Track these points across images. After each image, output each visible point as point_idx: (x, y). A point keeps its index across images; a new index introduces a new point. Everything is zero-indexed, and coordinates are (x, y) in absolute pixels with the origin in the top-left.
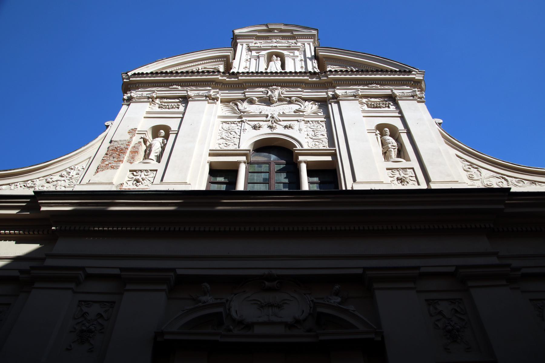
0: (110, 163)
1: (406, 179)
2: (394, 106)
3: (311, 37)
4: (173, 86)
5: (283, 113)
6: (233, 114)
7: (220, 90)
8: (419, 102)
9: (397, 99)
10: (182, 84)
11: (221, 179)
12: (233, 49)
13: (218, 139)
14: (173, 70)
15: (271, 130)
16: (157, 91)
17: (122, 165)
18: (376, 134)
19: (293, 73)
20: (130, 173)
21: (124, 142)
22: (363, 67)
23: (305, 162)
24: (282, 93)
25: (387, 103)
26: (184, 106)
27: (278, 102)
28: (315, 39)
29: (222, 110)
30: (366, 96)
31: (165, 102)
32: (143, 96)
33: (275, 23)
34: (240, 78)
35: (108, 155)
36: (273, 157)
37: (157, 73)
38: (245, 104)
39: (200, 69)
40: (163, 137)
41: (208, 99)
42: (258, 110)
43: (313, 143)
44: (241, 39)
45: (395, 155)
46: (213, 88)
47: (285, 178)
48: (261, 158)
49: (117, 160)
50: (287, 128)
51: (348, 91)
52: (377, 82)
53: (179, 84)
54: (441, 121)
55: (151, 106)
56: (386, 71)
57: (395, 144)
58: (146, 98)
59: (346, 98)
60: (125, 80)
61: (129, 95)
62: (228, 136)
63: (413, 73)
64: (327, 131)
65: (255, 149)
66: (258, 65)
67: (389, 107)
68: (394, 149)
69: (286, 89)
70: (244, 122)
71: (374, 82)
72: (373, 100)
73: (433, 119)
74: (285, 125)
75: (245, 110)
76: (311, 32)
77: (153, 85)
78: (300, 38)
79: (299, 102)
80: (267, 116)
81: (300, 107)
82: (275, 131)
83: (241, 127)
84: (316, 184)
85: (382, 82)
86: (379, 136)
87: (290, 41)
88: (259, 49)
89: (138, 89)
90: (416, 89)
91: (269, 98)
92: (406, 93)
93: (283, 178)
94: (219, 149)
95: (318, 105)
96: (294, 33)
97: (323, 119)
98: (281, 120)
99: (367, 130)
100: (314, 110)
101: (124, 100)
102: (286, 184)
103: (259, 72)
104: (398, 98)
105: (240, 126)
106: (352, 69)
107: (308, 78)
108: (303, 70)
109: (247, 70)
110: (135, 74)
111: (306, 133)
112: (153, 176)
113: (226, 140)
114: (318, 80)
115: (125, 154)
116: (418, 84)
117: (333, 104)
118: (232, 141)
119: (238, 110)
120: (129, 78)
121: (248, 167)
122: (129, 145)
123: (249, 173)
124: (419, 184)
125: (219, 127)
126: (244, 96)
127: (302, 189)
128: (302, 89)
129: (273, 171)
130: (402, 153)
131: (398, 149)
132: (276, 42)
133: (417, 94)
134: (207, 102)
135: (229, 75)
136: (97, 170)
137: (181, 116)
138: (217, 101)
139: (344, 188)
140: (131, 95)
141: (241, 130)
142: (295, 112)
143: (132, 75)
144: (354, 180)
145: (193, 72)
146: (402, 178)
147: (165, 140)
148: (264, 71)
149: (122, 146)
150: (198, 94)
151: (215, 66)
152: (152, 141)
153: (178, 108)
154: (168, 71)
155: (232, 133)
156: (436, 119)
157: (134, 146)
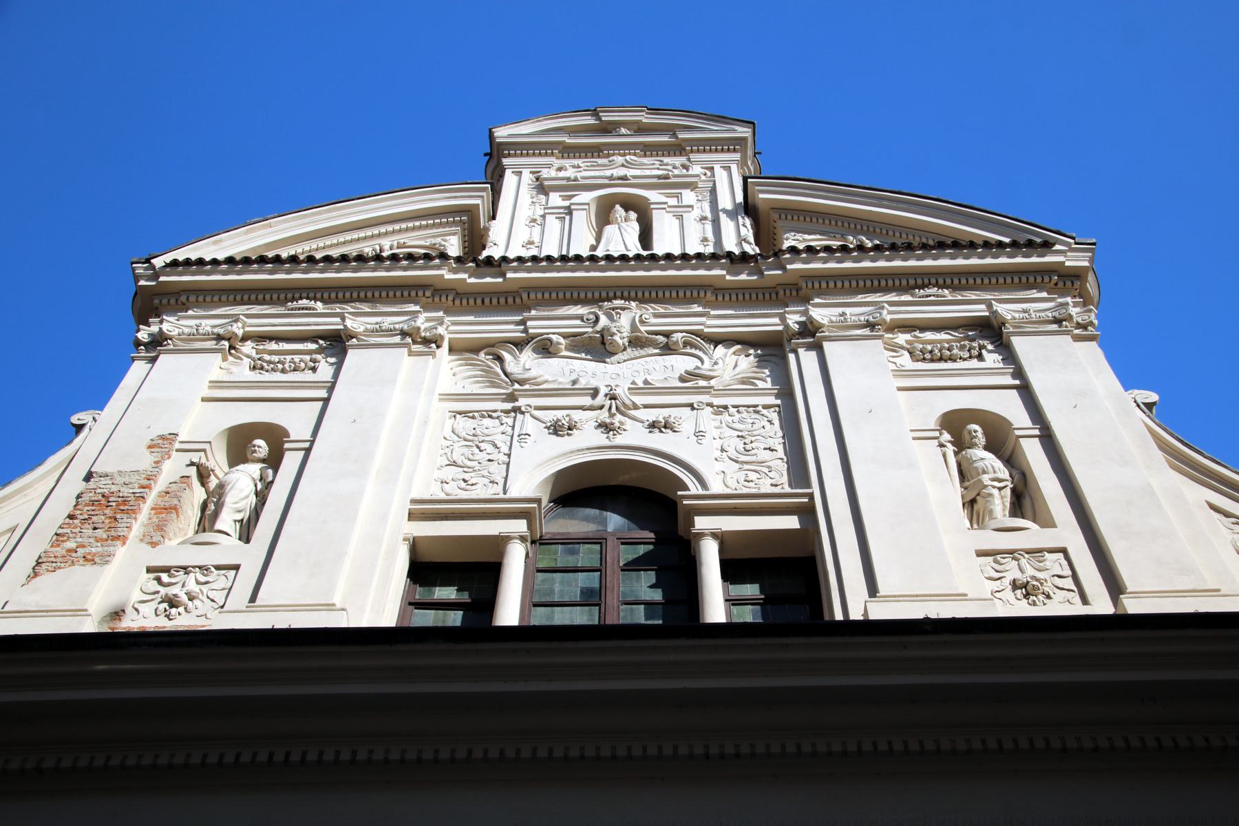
0: (84, 546)
1: (1042, 584)
2: (997, 355)
3: (732, 147)
4: (300, 302)
5: (646, 382)
7: (448, 312)
8: (1077, 338)
9: (1007, 332)
10: (326, 295)
11: (445, 593)
12: (489, 186)
13: (438, 465)
14: (300, 250)
15: (607, 437)
17: (121, 553)
19: (676, 258)
20: (145, 576)
21: (134, 478)
22: (897, 234)
23: (715, 535)
24: (642, 322)
25: (975, 344)
26: (332, 364)
27: (629, 350)
28: (746, 152)
29: (454, 375)
31: (271, 353)
33: (622, 108)
34: (510, 275)
35: (76, 518)
36: (614, 521)
39: (387, 247)
40: (263, 461)
41: (409, 340)
42: (567, 373)
43: (742, 476)
44: (515, 155)
45: (1004, 510)
46: (426, 308)
47: (651, 587)
48: (578, 523)
49: (105, 536)
51: (848, 311)
52: (941, 281)
54: (1153, 397)
55: (224, 365)
56: (944, 244)
57: (1004, 473)
59: (844, 332)
60: (142, 283)
61: (154, 329)
62: (471, 457)
63: (1058, 247)
64: (783, 437)
65: (553, 499)
67: (980, 357)
68: (1000, 489)
69: (655, 309)
70: (523, 413)
71: (933, 281)
72: (929, 336)
73: (1126, 390)
74: (652, 418)
75: (526, 376)
76: (735, 131)
77: (235, 299)
78: (698, 151)
79: (696, 347)
80: (595, 393)
81: (699, 364)
82: (619, 440)
83: (513, 427)
84: (752, 604)
85: (956, 281)
86: (950, 449)
87: (666, 160)
89: (186, 312)
90: (1069, 300)
91: (602, 336)
92: (1035, 311)
93: (645, 587)
94: (442, 496)
95: (756, 356)
96: (680, 136)
99: (911, 431)
100: (742, 373)
101: (138, 343)
104: (1011, 330)
105: (511, 424)
107: (724, 272)
108: (710, 249)
109: (534, 252)
110: (175, 263)
111: (718, 443)
112: (223, 586)
113: (465, 469)
114: (755, 278)
115: (134, 515)
116: (1075, 282)
117: (801, 351)
118: (485, 472)
119: (503, 376)
120: (155, 276)
121: (535, 554)
122: (149, 487)
123: (539, 571)
124: (1085, 601)
125: (443, 429)
126: (522, 332)
128: (704, 307)
129: (613, 563)
130: (1027, 503)
131: (1013, 491)
132: (623, 165)
133: (1072, 313)
134: (406, 349)
135: (477, 265)
136: (34, 568)
138: (438, 347)
139: (839, 616)
140: (161, 329)
141: (512, 436)
142: (682, 379)
143: (167, 265)
144: (873, 589)
145: (361, 258)
146: (1028, 582)
147: (270, 472)
148: (585, 253)
149: (126, 491)
151: (433, 241)
152: (226, 474)
153: (314, 369)
154: (284, 255)
155: (483, 446)
156: (1136, 392)
157: (164, 489)
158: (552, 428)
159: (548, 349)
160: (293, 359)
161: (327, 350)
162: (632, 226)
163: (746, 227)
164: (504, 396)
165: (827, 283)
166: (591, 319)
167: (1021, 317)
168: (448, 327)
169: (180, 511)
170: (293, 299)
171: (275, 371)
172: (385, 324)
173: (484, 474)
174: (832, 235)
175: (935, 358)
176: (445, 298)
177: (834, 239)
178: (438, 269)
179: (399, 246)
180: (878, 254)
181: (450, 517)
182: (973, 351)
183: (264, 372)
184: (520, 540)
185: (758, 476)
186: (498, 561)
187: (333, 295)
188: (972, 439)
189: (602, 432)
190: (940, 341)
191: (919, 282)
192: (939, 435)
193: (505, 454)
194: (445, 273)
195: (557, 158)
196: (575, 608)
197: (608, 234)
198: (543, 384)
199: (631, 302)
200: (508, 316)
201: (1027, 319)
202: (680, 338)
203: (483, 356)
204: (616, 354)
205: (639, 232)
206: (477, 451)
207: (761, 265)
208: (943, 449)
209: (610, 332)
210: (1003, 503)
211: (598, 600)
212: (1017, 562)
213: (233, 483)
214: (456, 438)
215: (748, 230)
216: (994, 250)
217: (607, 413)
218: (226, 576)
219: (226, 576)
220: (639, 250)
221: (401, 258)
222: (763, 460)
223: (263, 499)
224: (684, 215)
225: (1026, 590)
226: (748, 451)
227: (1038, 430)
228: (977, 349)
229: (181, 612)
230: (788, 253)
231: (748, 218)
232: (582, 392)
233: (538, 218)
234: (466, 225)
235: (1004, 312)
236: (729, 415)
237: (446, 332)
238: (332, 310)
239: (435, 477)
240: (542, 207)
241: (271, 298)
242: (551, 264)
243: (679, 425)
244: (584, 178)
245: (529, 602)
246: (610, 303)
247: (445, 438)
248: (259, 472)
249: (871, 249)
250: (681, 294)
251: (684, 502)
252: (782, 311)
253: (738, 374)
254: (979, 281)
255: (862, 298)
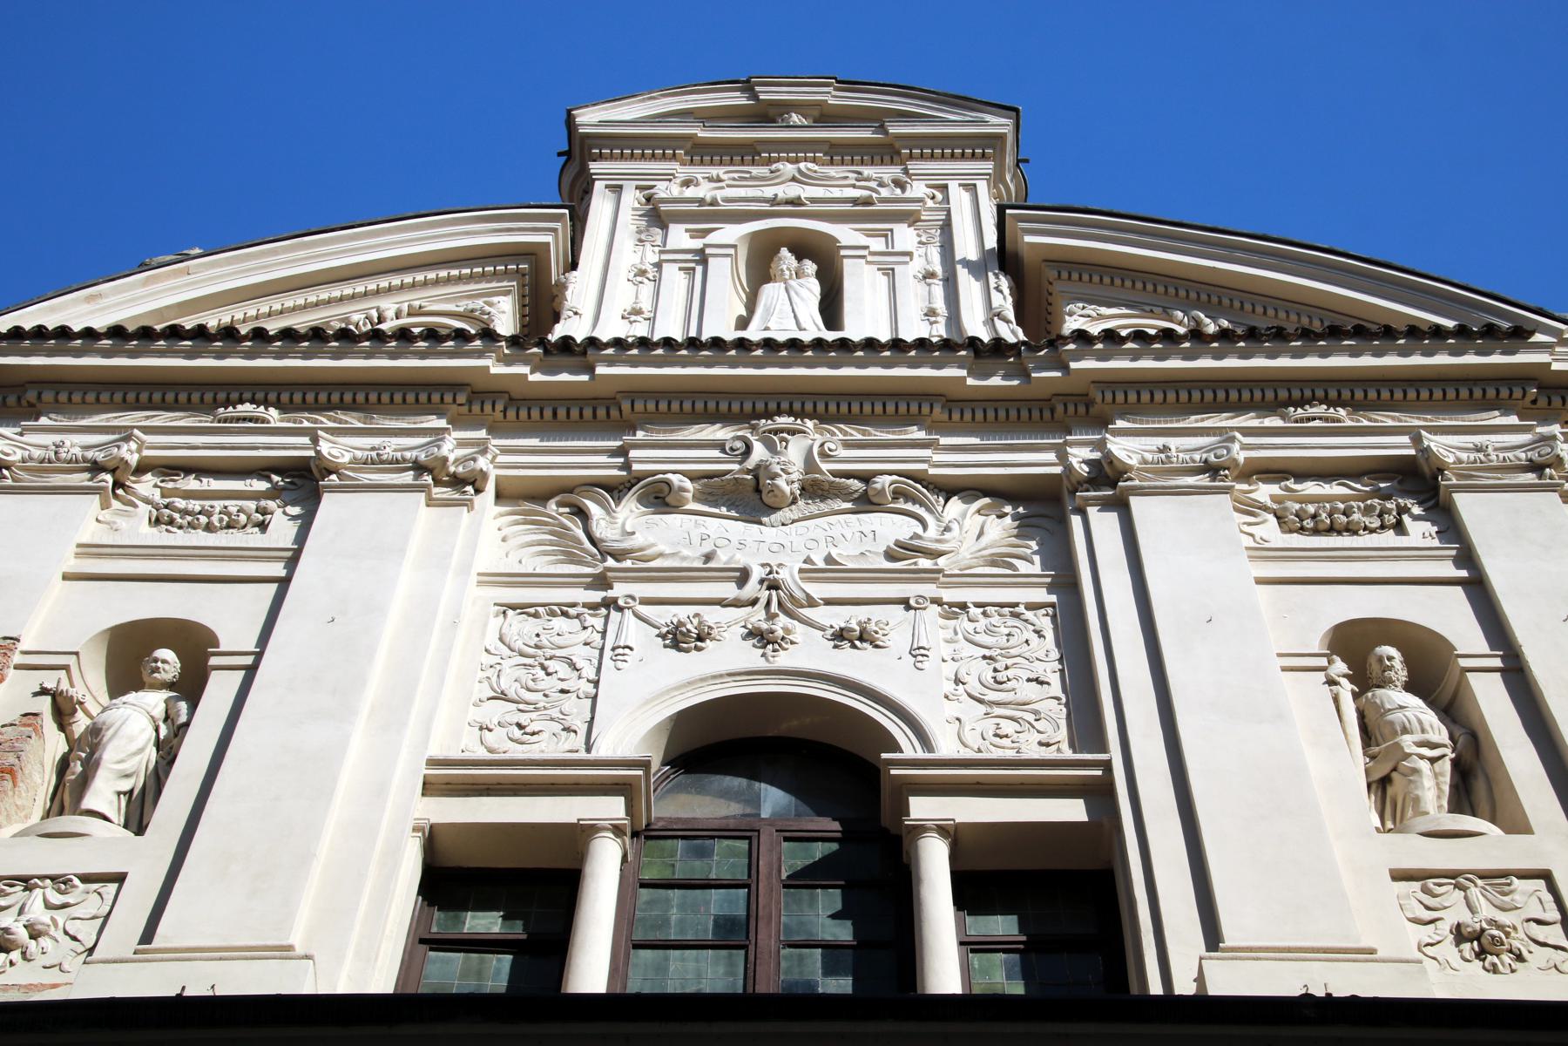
1: (1507, 935)
3: (979, 151)
4: (240, 407)
5: (829, 559)
6: (562, 562)
7: (494, 430)
9: (1445, 486)
10: (285, 397)
11: (483, 922)
12: (567, 211)
13: (475, 698)
15: (763, 655)
16: (141, 428)
18: (1326, 676)
22: (1259, 310)
23: (943, 830)
24: (825, 456)
25: (1390, 505)
26: (294, 518)
27: (801, 503)
29: (504, 540)
30: (1276, 466)
32: (63, 455)
34: (601, 370)
36: (773, 799)
37: (146, 333)
38: (630, 511)
39: (390, 314)
40: (170, 686)
41: (428, 479)
42: (696, 540)
43: (989, 726)
44: (611, 157)
45: (1439, 797)
46: (457, 423)
47: (833, 917)
50: (851, 641)
51: (1173, 442)
52: (1333, 394)
53: (272, 397)
55: (106, 515)
56: (1384, 334)
57: (1439, 732)
58: (728, 579)
62: (531, 684)
63: (1539, 337)
64: (1060, 660)
65: (670, 758)
66: (698, 302)
67: (1399, 528)
68: (1433, 760)
69: (846, 433)
70: (620, 609)
71: (1320, 393)
72: (1311, 488)
74: (839, 623)
75: (626, 545)
77: (124, 400)
78: (922, 157)
79: (915, 501)
80: (743, 577)
81: (919, 530)
82: (783, 660)
83: (604, 633)
84: (1005, 951)
85: (1359, 395)
86: (1346, 689)
87: (868, 171)
88: (706, 215)
89: (37, 419)
91: (756, 478)
92: (1496, 449)
94: (481, 753)
95: (1016, 517)
96: (892, 131)
97: (1041, 595)
98: (815, 596)
99: (1280, 655)
102: (837, 952)
103: (704, 338)
104: (1455, 481)
105: (600, 628)
106: (1198, 322)
107: (964, 373)
108: (939, 331)
109: (641, 330)
111: (949, 669)
112: (94, 912)
113: (521, 706)
114: (1016, 382)
117: (1092, 512)
118: (555, 713)
121: (638, 855)
123: (643, 885)
125: (484, 634)
126: (620, 468)
127: (923, 988)
128: (929, 430)
129: (770, 875)
130: (1480, 787)
131: (1456, 763)
132: (794, 179)
134: (424, 494)
135: (547, 352)
137: (278, 570)
138: (478, 491)
141: (602, 649)
142: (890, 556)
144: (1212, 936)
146: (1483, 930)
147: (183, 706)
148: (730, 335)
150: (374, 454)
151: (471, 304)
152: (105, 709)
153: (263, 526)
158: (671, 636)
159: (664, 498)
160: (226, 507)
161: (284, 493)
162: (808, 285)
163: (1001, 292)
164: (589, 580)
165: (1139, 394)
166: (738, 449)
167: (1472, 458)
168: (494, 457)
169: (19, 775)
170: (227, 403)
171: (194, 528)
172: (388, 450)
173: (554, 715)
174: (1148, 308)
175: (1321, 527)
176: (490, 407)
177: (1150, 314)
178: (479, 357)
179: (411, 311)
180: (1227, 346)
181: (492, 790)
182: (1386, 516)
183: (175, 530)
184: (614, 833)
185: (1017, 727)
186: (578, 867)
187: (298, 397)
188: (1384, 671)
189: (754, 646)
190: (1330, 499)
191: (1296, 394)
192: (1327, 664)
193: (588, 681)
194: (490, 365)
195: (682, 164)
196: (705, 951)
197: (767, 299)
198: (655, 559)
199: (806, 420)
200: (597, 440)
201: (1481, 462)
202: (887, 486)
203: (554, 507)
204: (780, 509)
205: (819, 297)
206: (541, 674)
207: (1025, 361)
208: (1333, 688)
209: (769, 471)
210: (1438, 784)
211: (744, 939)
212: (1462, 893)
213: (117, 725)
214: (506, 652)
215: (1005, 298)
216: (1427, 342)
217: (764, 612)
218: (99, 894)
219: (99, 894)
220: (819, 330)
221: (416, 337)
222: (1026, 699)
223: (169, 754)
224: (898, 269)
225: (1480, 944)
226: (1001, 683)
227: (1499, 660)
228: (1395, 513)
229: (14, 961)
230: (1073, 343)
231: (1005, 276)
232: (722, 574)
233: (649, 268)
234: (527, 277)
235: (1441, 450)
236: (970, 620)
237: (491, 466)
238: (295, 423)
239: (470, 718)
240: (657, 249)
241: (189, 399)
242: (670, 353)
243: (884, 635)
244: (728, 200)
245: (626, 942)
246: (769, 422)
247: (486, 650)
248: (163, 706)
249: (1214, 337)
250: (891, 408)
251: (893, 772)
252: (1061, 441)
253: (984, 549)
254: (1398, 395)
255: (1197, 421)
